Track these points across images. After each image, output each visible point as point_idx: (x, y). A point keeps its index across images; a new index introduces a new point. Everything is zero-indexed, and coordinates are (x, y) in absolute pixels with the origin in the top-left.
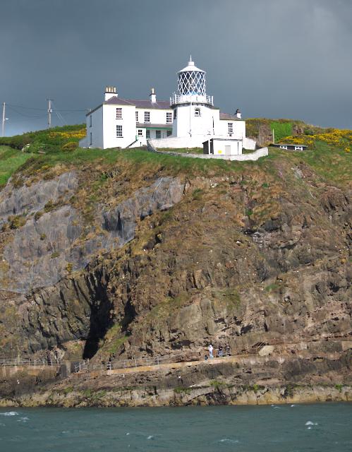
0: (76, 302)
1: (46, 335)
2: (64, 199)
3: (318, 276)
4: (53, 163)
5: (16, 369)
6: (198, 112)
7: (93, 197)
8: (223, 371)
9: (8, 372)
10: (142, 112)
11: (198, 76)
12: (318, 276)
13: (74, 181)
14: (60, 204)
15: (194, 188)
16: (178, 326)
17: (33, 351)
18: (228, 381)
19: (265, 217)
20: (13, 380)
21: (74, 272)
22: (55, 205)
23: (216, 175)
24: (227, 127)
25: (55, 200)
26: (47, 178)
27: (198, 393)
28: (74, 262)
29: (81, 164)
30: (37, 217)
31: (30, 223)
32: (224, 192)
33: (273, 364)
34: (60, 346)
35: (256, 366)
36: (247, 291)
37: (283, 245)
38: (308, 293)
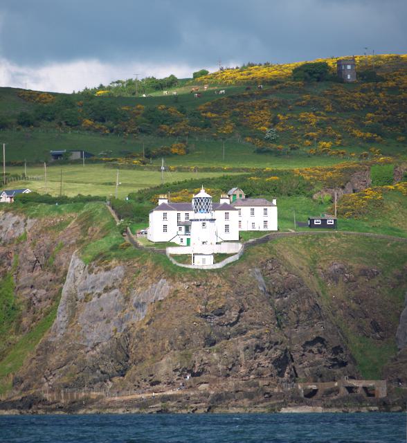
0: (119, 352)
1: (102, 372)
2: (115, 284)
3: (249, 342)
4: (112, 259)
5: (83, 394)
6: (204, 224)
7: (131, 285)
8: (171, 399)
9: (77, 396)
10: (183, 214)
11: (205, 201)
12: (249, 342)
13: (122, 272)
14: (113, 288)
15: (175, 289)
16: (153, 373)
17: (95, 383)
18: (172, 404)
19: (215, 307)
20: (81, 401)
21: (117, 333)
22: (110, 288)
23: (188, 281)
24: (250, 211)
25: (110, 285)
26: (107, 269)
27: (153, 410)
28: (118, 327)
29: (127, 261)
30: (99, 295)
31: (94, 299)
32: (191, 292)
33: (207, 395)
34: (110, 380)
35: (194, 396)
36: (197, 353)
37: (226, 323)
38: (241, 352)
